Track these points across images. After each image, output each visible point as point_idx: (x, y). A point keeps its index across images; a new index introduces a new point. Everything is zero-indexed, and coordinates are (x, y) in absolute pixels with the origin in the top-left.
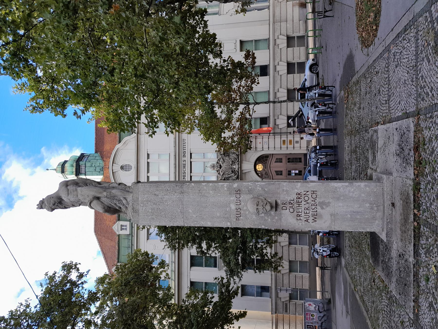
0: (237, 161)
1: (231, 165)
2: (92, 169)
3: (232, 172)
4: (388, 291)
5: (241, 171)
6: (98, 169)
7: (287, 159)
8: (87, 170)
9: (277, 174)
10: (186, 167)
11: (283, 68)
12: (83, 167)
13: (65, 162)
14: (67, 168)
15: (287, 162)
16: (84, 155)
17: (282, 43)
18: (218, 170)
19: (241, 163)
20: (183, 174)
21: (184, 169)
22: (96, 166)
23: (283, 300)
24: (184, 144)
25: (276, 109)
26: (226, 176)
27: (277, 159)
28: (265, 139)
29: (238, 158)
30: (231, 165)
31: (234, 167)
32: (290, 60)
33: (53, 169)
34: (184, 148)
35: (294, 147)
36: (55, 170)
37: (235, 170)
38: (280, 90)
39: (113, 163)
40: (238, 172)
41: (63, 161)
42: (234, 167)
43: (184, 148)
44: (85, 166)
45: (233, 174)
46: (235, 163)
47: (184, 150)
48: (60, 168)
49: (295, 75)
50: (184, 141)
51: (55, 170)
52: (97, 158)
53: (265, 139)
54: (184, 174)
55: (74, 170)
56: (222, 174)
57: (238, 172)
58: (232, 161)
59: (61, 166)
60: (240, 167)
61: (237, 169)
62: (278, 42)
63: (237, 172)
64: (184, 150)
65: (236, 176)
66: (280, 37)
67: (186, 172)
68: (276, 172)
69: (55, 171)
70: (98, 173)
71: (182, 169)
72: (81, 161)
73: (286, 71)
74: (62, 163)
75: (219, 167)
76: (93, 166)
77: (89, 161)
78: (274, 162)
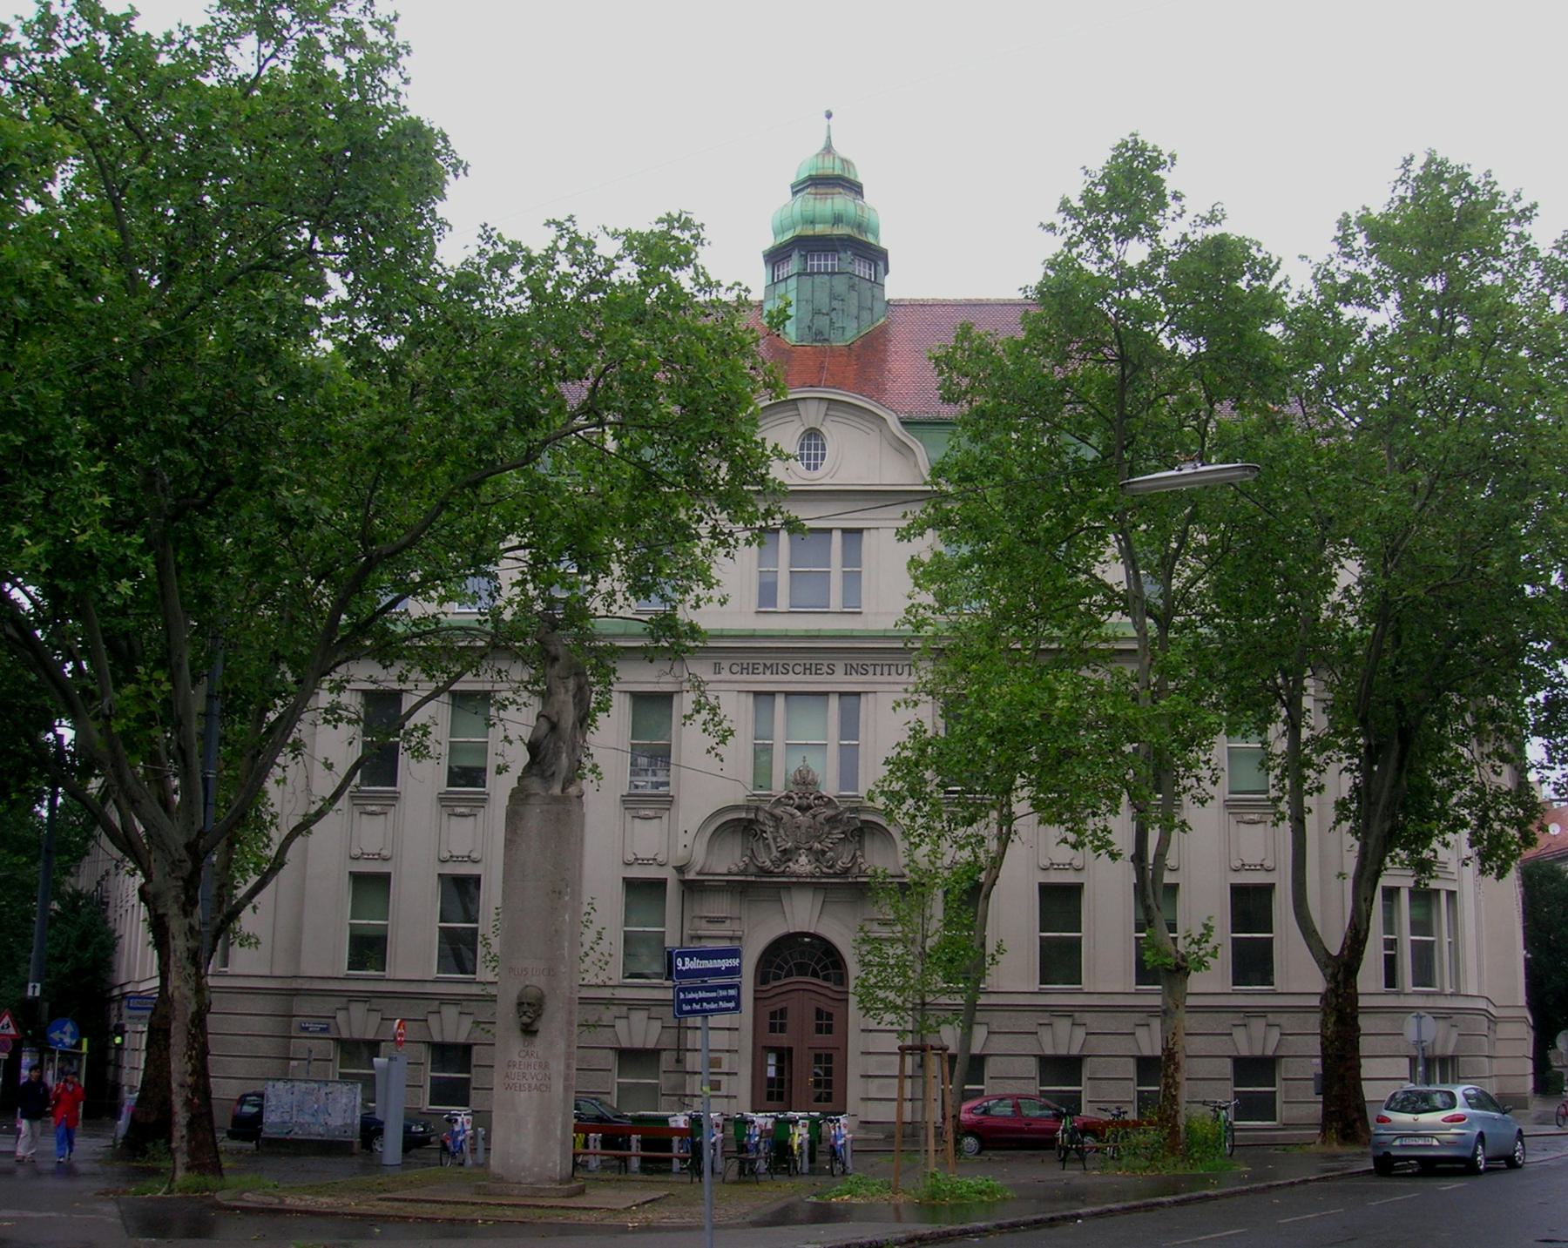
0: (825, 870)
1: (807, 846)
2: (823, 300)
3: (785, 852)
4: (260, 572)
5: (788, 886)
6: (822, 322)
7: (829, 1052)
8: (818, 279)
9: (773, 1015)
10: (808, 678)
11: (1063, 1040)
12: (828, 263)
13: (856, 189)
14: (829, 201)
15: (818, 1051)
16: (881, 265)
17: (1250, 1040)
18: (791, 798)
19: (816, 887)
20: (781, 662)
21: (802, 669)
22: (833, 314)
23: (341, 1016)
24: (893, 669)
25: (1012, 1014)
26: (769, 830)
27: (830, 1016)
28: (265, 1046)
29: (836, 875)
30: (810, 849)
31: (803, 859)
32: (1283, 1071)
33: (829, 137)
34: (878, 669)
35: (728, 1051)
36: (828, 149)
37: (790, 860)
38: (1080, 1033)
39: (830, 400)
40: (784, 872)
41: (860, 179)
42: (803, 859)
43: (878, 669)
44: (833, 273)
45: (775, 853)
46: (817, 860)
47: (871, 669)
48: (829, 172)
49: (1231, 1083)
50: (907, 668)
51: (828, 149)
52: (865, 315)
53: (265, 1046)
54: (780, 667)
55: (820, 229)
56: (778, 811)
57: (783, 874)
58: (823, 853)
59: (838, 172)
60: (801, 880)
61: (793, 867)
62: (1258, 1025)
63: (782, 869)
64: (871, 669)
65: (768, 863)
66: (1275, 1034)
67: (791, 677)
68: (783, 1013)
69: (822, 145)
70: (807, 321)
71: (802, 662)
72: (855, 254)
73: (1049, 1051)
74: (852, 177)
75: (805, 802)
76: (836, 304)
77: (852, 287)
78: (821, 1006)
